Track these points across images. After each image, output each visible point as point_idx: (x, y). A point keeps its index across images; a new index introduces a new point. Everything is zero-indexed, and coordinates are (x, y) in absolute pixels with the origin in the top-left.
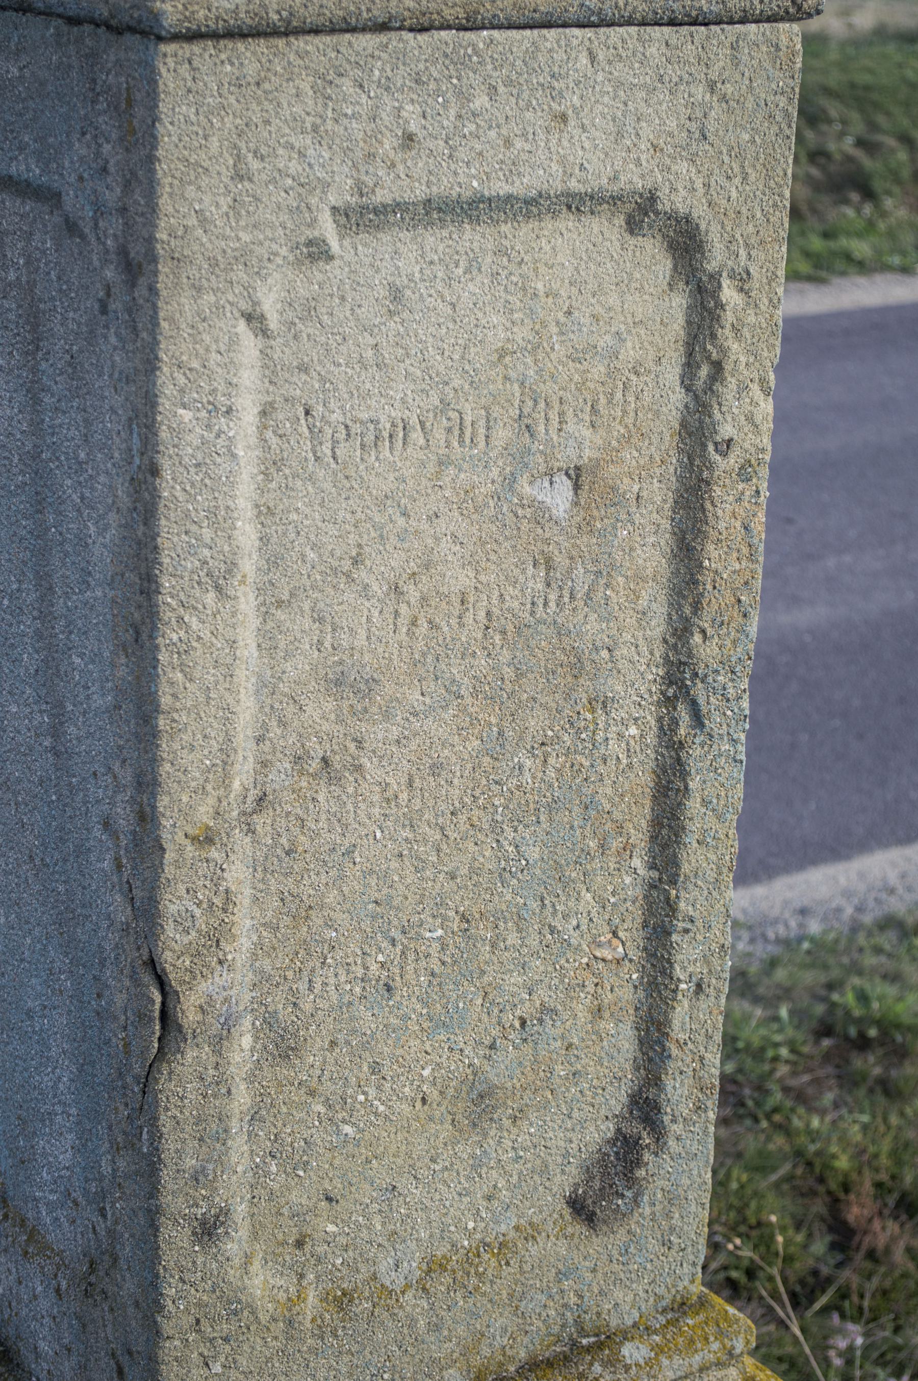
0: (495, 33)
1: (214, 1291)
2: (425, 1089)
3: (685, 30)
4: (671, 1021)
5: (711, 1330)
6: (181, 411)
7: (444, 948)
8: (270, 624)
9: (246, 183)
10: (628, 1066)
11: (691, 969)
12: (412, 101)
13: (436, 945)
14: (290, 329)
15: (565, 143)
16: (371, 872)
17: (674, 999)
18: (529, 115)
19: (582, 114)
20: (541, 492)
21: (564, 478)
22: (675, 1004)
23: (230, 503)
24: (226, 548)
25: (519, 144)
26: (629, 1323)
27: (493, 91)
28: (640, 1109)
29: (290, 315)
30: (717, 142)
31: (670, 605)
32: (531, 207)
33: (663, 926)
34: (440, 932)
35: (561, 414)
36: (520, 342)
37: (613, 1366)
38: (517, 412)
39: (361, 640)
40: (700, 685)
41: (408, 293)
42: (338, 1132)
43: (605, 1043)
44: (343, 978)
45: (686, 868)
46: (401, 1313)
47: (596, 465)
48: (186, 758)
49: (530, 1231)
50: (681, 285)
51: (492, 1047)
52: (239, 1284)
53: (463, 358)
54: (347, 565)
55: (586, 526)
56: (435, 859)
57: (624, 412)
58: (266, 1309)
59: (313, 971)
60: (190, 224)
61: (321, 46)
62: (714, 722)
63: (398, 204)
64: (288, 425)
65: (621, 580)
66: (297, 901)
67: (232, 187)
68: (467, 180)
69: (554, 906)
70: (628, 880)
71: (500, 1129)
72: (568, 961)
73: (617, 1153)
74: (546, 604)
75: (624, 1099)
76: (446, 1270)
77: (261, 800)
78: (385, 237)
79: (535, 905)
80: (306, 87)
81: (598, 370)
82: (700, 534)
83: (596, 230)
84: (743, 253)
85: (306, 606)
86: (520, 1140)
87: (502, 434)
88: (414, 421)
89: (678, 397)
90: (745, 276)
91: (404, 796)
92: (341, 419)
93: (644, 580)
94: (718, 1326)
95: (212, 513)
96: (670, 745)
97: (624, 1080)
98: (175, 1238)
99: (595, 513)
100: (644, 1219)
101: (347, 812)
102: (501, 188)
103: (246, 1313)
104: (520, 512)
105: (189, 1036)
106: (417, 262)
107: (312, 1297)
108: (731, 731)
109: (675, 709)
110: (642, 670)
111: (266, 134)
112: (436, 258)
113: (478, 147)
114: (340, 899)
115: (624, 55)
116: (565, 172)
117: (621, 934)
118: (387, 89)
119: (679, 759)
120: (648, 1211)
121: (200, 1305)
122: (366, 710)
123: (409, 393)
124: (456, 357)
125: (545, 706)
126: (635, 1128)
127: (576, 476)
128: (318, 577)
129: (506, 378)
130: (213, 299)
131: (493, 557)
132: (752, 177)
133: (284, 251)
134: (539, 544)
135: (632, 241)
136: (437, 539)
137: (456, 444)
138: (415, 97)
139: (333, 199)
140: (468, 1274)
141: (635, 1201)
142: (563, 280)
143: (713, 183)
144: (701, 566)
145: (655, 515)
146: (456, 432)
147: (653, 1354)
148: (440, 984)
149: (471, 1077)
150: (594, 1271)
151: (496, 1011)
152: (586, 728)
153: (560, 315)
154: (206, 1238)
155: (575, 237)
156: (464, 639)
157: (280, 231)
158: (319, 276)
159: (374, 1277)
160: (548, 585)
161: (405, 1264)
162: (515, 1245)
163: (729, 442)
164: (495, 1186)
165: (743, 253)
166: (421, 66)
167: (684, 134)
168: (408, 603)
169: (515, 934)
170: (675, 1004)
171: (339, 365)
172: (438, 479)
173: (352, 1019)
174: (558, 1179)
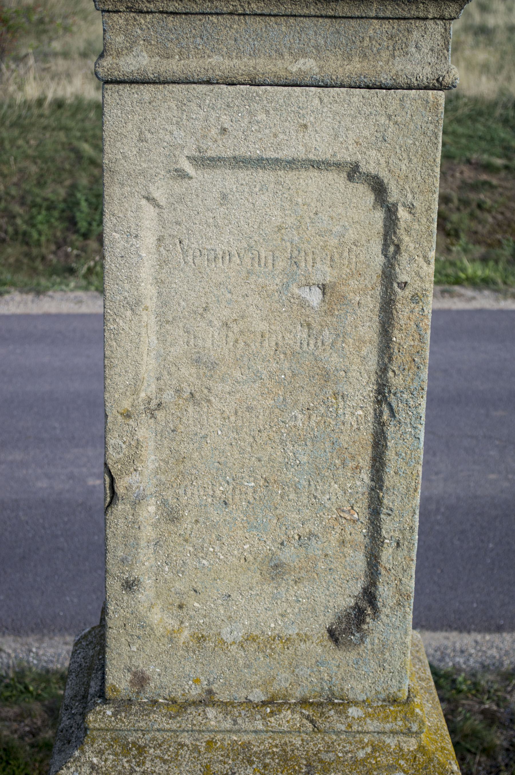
0: (269, 88)
1: (132, 614)
2: (245, 554)
3: (373, 91)
4: (380, 557)
5: (400, 716)
6: (114, 234)
7: (255, 492)
9: (144, 143)
10: (362, 573)
11: (392, 534)
12: (225, 114)
13: (250, 491)
15: (307, 138)
16: (216, 449)
17: (382, 546)
18: (287, 124)
19: (315, 126)
20: (305, 293)
21: (318, 289)
22: (383, 549)
23: (138, 275)
24: (136, 293)
25: (281, 136)
26: (361, 699)
27: (267, 112)
28: (368, 596)
29: (172, 200)
30: (392, 143)
31: (379, 356)
32: (292, 164)
33: (377, 510)
34: (253, 484)
35: (314, 259)
36: (290, 224)
37: (340, 714)
38: (290, 255)
39: (209, 344)
40: (393, 397)
41: (230, 196)
42: (200, 562)
43: (348, 559)
44: (202, 493)
45: (386, 483)
46: (229, 654)
47: (334, 285)
48: (117, 378)
49: (304, 637)
50: (379, 207)
51: (282, 544)
53: (259, 228)
54: (201, 311)
55: (330, 312)
56: (250, 450)
57: (349, 262)
58: (160, 631)
59: (186, 486)
60: (118, 157)
61: (180, 89)
62: (401, 416)
63: (219, 158)
64: (171, 246)
65: (351, 341)
66: (178, 453)
67: (138, 144)
68: (254, 150)
69: (316, 486)
70: (359, 483)
71: (287, 584)
72: (324, 514)
73: (355, 614)
74: (308, 345)
75: (360, 589)
76: (255, 641)
77: (159, 405)
78: (218, 171)
79: (305, 484)
80: (173, 105)
81: (333, 242)
82: (391, 325)
83: (331, 177)
84: (410, 196)
85: (181, 325)
86: (298, 592)
87: (281, 264)
88: (234, 252)
89: (380, 259)
91: (233, 419)
92: (197, 247)
93: (364, 342)
94: (406, 715)
95: (129, 278)
96: (379, 424)
97: (359, 580)
98: (114, 586)
99: (334, 307)
100: (367, 650)
101: (203, 419)
102: (273, 155)
103: (148, 628)
104: (292, 300)
105: (120, 499)
107: (186, 633)
108: (412, 422)
109: (381, 406)
110: (364, 384)
111: (154, 124)
112: (244, 183)
113: (260, 136)
114: (200, 457)
115: (338, 100)
116: (306, 151)
117: (355, 508)
118: (213, 109)
119: (383, 430)
120: (369, 647)
121: (125, 617)
122: (212, 376)
123: (231, 240)
124: (256, 227)
125: (309, 392)
126: (364, 604)
127: (323, 288)
128: (187, 314)
129: (282, 239)
130: (129, 189)
131: (278, 318)
132: (415, 160)
133: (163, 173)
134: (303, 316)
135: (351, 185)
136: (248, 306)
137: (257, 265)
138: (227, 113)
139: (186, 152)
140: (266, 646)
141: (362, 640)
142: (312, 199)
143: (391, 162)
144: (391, 340)
145: (370, 313)
146: (257, 260)
147: (364, 716)
148: (253, 508)
149: (270, 556)
150: (338, 666)
151: (284, 528)
152: (332, 406)
153: (311, 215)
154: (128, 589)
155: (319, 180)
156: (263, 353)
157: (161, 164)
158: (186, 185)
159: (219, 634)
160: (309, 336)
161: (235, 633)
162: (294, 641)
163: (406, 283)
164: (286, 611)
165: (410, 196)
166: (230, 100)
167: (374, 138)
168: (233, 332)
169: (294, 495)
170: (383, 549)
171: (196, 224)
172: (247, 280)
173: (206, 513)
174: (322, 617)
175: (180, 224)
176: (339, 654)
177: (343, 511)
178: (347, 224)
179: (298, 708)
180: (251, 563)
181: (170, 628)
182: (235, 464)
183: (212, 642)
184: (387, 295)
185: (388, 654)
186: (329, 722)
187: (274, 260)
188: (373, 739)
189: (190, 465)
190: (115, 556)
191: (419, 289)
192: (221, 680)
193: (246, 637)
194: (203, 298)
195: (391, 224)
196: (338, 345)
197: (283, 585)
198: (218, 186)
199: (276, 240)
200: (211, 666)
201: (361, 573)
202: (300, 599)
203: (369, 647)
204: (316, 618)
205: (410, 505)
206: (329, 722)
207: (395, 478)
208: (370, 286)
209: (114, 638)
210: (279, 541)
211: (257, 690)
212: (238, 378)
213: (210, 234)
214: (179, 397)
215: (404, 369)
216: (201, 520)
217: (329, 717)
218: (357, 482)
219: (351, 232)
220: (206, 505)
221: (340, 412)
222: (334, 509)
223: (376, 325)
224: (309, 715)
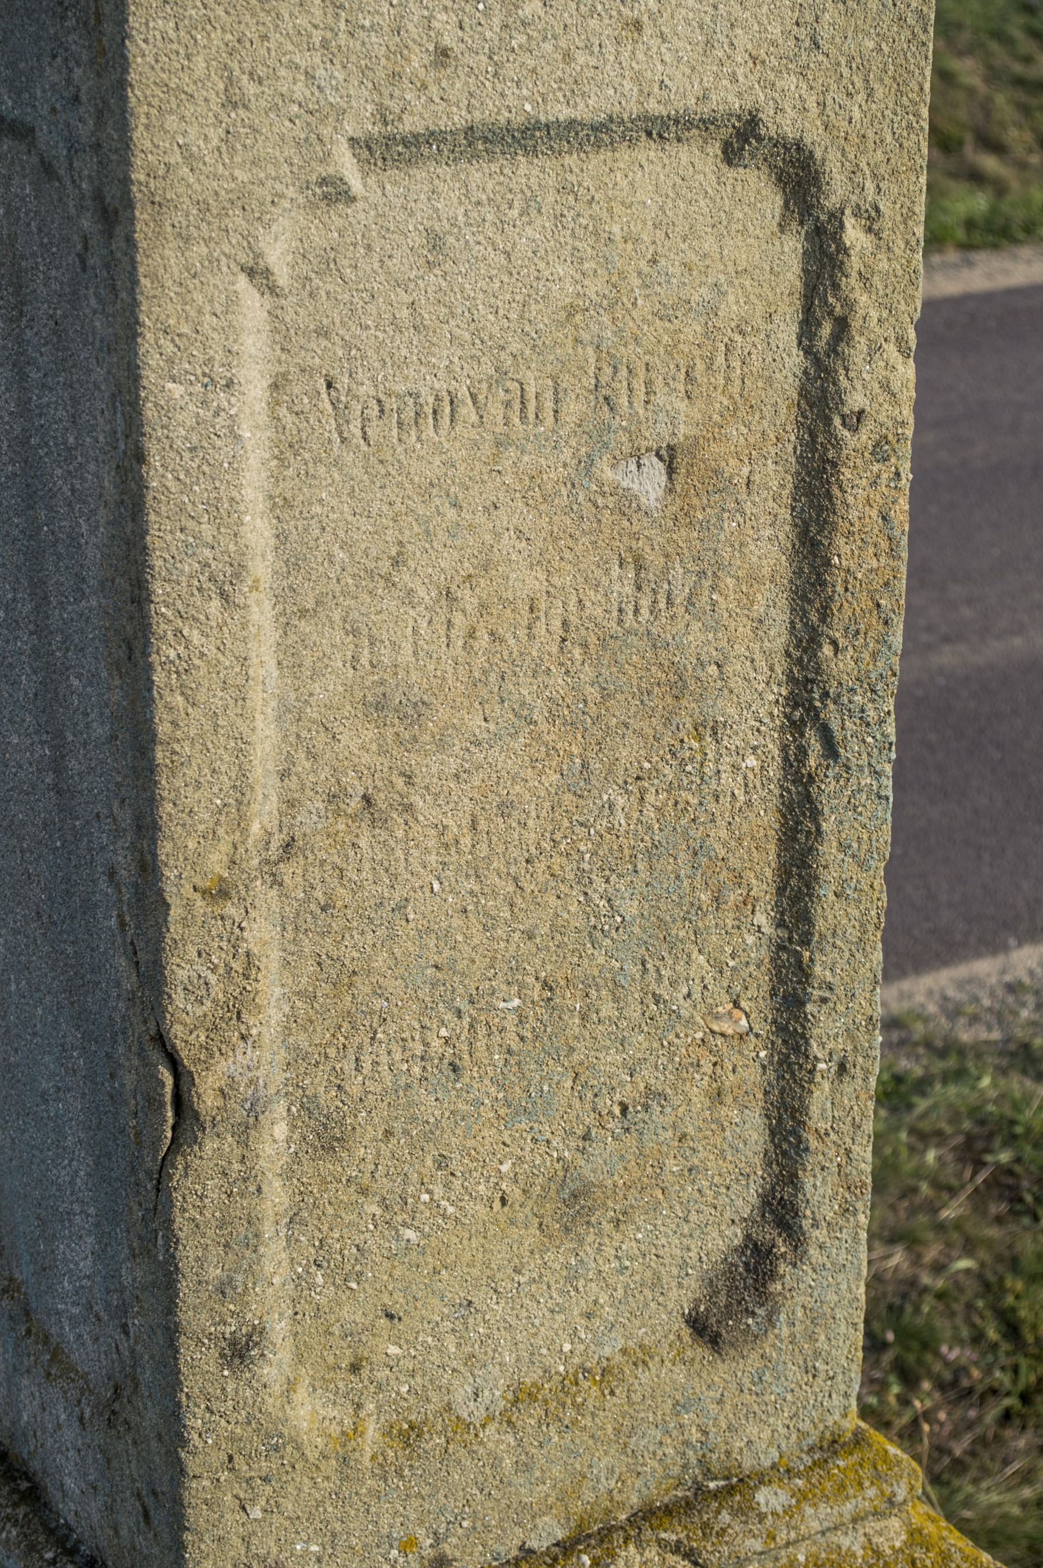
1: (249, 1423)
2: (504, 1187)
5: (866, 1473)
6: (170, 385)
7: (522, 1020)
8: (292, 638)
9: (241, 111)
13: (512, 1018)
14: (304, 286)
15: (640, 56)
16: (429, 930)
18: (593, 23)
19: (660, 21)
20: (626, 477)
21: (655, 460)
23: (235, 494)
24: (232, 548)
25: (581, 58)
28: (772, 1212)
29: (304, 268)
30: (833, 51)
31: (793, 610)
32: (600, 134)
34: (516, 1002)
35: (649, 383)
37: (744, 1514)
38: (593, 381)
39: (406, 655)
40: (832, 706)
41: (451, 240)
42: (398, 1237)
43: (728, 1133)
44: (398, 1056)
45: (820, 925)
48: (190, 797)
49: (640, 1355)
50: (794, 226)
51: (586, 1137)
52: (280, 1415)
53: (522, 317)
54: (385, 566)
55: (684, 517)
56: (508, 915)
57: (728, 379)
58: (314, 1444)
59: (360, 1047)
60: (172, 161)
63: (432, 134)
64: (306, 400)
66: (338, 965)
68: (516, 103)
69: (658, 970)
70: (750, 940)
71: (600, 1234)
72: (677, 1036)
73: (746, 1264)
74: (636, 611)
75: (754, 1200)
77: (288, 846)
78: (419, 174)
79: (635, 970)
81: (693, 330)
82: (824, 525)
84: (870, 186)
85: (336, 616)
86: (624, 1247)
87: (573, 409)
89: (795, 360)
90: (873, 214)
91: (466, 841)
92: (372, 392)
94: (875, 1468)
95: (213, 506)
98: (199, 1363)
99: (695, 501)
105: (208, 1124)
106: (461, 203)
107: (372, 1430)
108: (874, 762)
109: (802, 735)
110: (760, 689)
112: (484, 197)
113: (531, 63)
117: (743, 1004)
119: (808, 797)
120: (785, 1332)
121: (232, 1439)
122: (415, 739)
123: (456, 360)
124: (513, 316)
126: (769, 1234)
127: (669, 458)
128: (350, 581)
130: (204, 250)
131: (568, 555)
132: (880, 92)
133: (291, 192)
134: (625, 539)
135: (731, 173)
136: (497, 535)
137: (517, 421)
139: (350, 128)
141: (770, 1320)
143: (829, 101)
144: (828, 563)
146: (517, 406)
147: (794, 1501)
148: (519, 1064)
150: (720, 1402)
151: (590, 1095)
154: (237, 1361)
155: (658, 169)
158: (339, 222)
159: (448, 1407)
162: (622, 1371)
163: (861, 412)
164: (596, 1302)
165: (870, 186)
167: (791, 43)
169: (611, 1004)
171: (367, 328)
173: (411, 1104)
174: (674, 1293)
175: (327, 335)
176: (722, 1371)
177: (717, 1017)
178: (722, 278)
179: (648, 1534)
180: (517, 1207)
181: (335, 1430)
182: (473, 961)
183: (439, 1434)
184: (814, 450)
185: (823, 1337)
186: (727, 1543)
187: (557, 402)
188: (814, 1549)
189: (367, 989)
190: (200, 1282)
191: (890, 424)
192: (465, 1524)
193: (510, 1396)
194: (390, 532)
195: (823, 266)
196: (705, 599)
197: (590, 1239)
198: (419, 214)
199: (562, 345)
200: (440, 1496)
201: (757, 1160)
202: (627, 1263)
203: (785, 1332)
204: (661, 1299)
205: (868, 966)
206: (727, 1543)
207: (837, 907)
208: (772, 436)
209: (206, 1502)
210: (580, 1131)
211: (545, 1519)
212: (477, 731)
213: (404, 352)
214: (337, 813)
215: (858, 632)
216: (398, 1126)
217: (724, 1530)
218: (746, 936)
219: (731, 298)
220: (408, 1086)
221: (710, 769)
222: (698, 1019)
223: (785, 532)
224: (679, 1541)
